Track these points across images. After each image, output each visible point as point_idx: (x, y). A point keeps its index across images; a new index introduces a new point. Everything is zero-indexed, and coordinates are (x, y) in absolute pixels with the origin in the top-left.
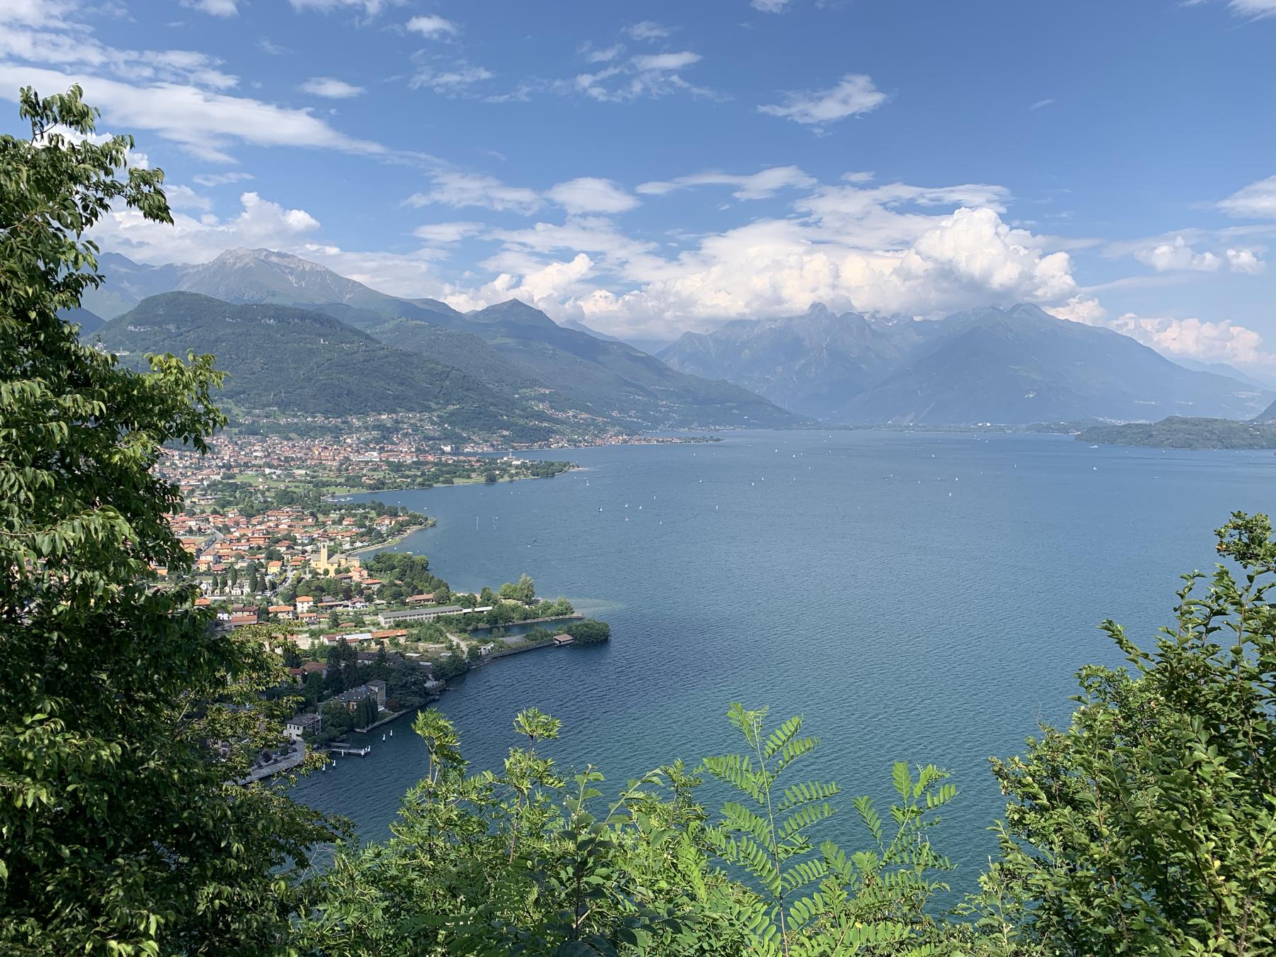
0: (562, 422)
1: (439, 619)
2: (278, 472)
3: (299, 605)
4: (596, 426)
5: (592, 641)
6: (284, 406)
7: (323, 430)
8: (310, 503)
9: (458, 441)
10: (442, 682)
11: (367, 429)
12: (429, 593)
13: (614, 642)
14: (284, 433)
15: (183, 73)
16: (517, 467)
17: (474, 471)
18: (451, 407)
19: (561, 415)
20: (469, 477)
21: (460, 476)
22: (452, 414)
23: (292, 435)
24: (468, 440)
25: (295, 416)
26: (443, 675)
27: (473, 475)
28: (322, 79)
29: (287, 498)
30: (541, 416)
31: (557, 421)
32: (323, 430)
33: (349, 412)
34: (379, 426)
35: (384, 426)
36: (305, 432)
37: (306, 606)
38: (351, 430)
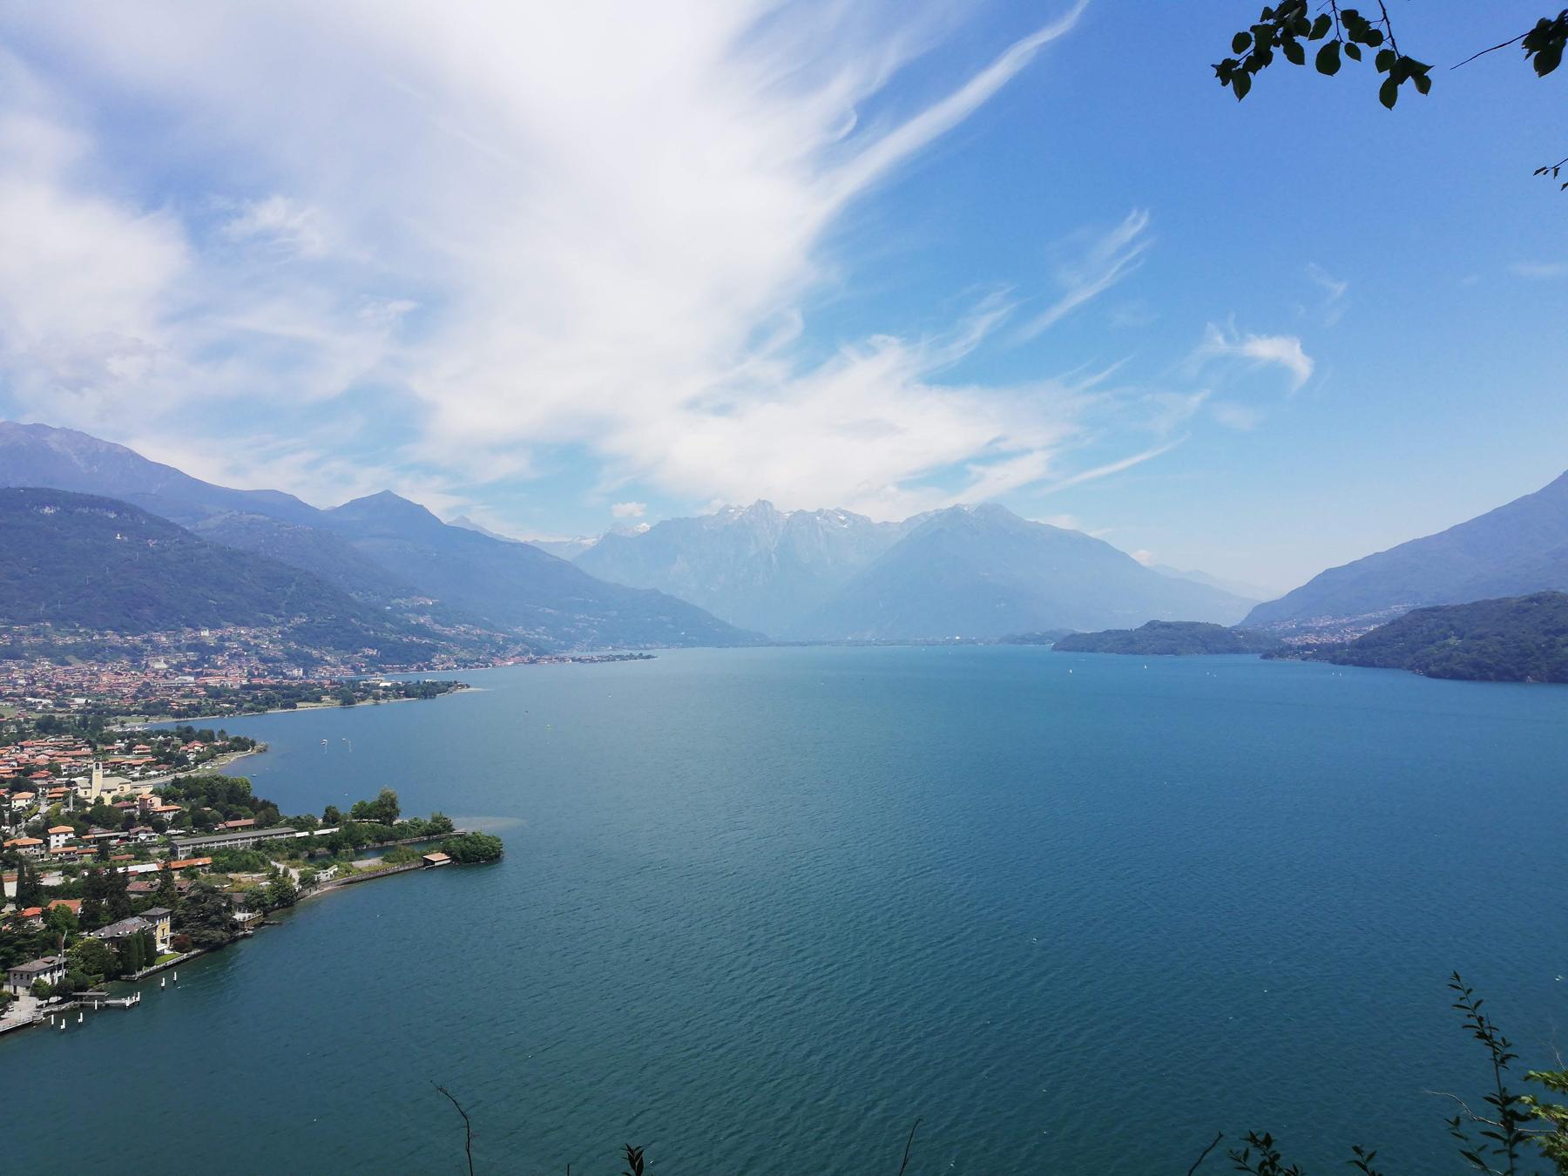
0: (448, 639)
1: (258, 845)
2: (45, 701)
3: (53, 839)
4: (493, 643)
5: (476, 856)
6: (62, 620)
7: (117, 651)
8: (91, 730)
9: (309, 663)
10: (257, 914)
11: (178, 649)
12: (247, 818)
13: (508, 859)
14: (59, 656)
15: (1527, 605)
16: (385, 688)
17: (327, 694)
18: (297, 620)
19: (447, 631)
20: (318, 700)
21: (305, 700)
22: (298, 629)
23: (71, 658)
24: (321, 661)
25: (77, 634)
26: (259, 905)
27: (325, 698)
28: (877, 339)
29: (47, 726)
30: (420, 630)
31: (440, 637)
32: (117, 651)
33: (153, 627)
34: (200, 647)
35: (204, 644)
36: (90, 653)
37: (63, 838)
38: (159, 650)
